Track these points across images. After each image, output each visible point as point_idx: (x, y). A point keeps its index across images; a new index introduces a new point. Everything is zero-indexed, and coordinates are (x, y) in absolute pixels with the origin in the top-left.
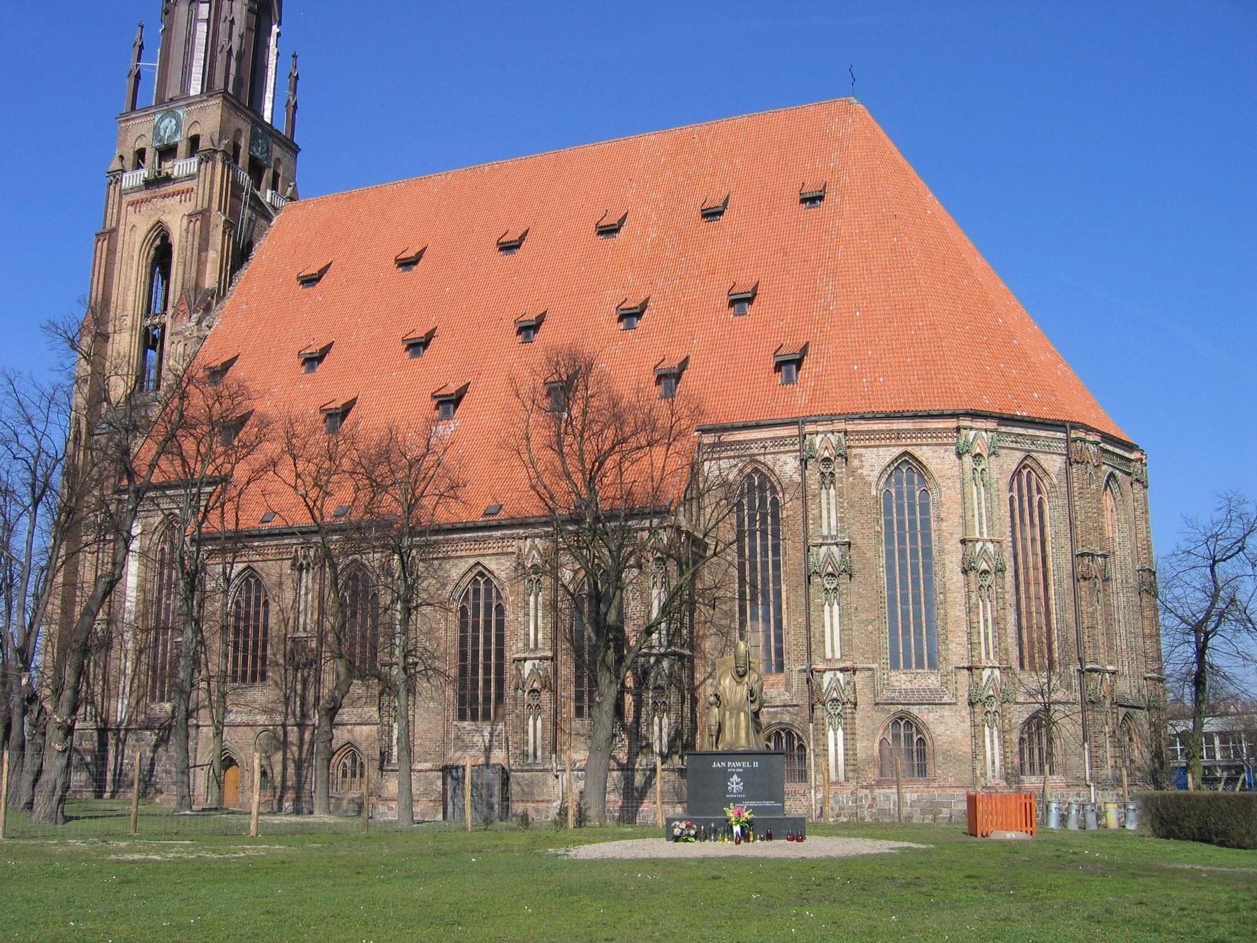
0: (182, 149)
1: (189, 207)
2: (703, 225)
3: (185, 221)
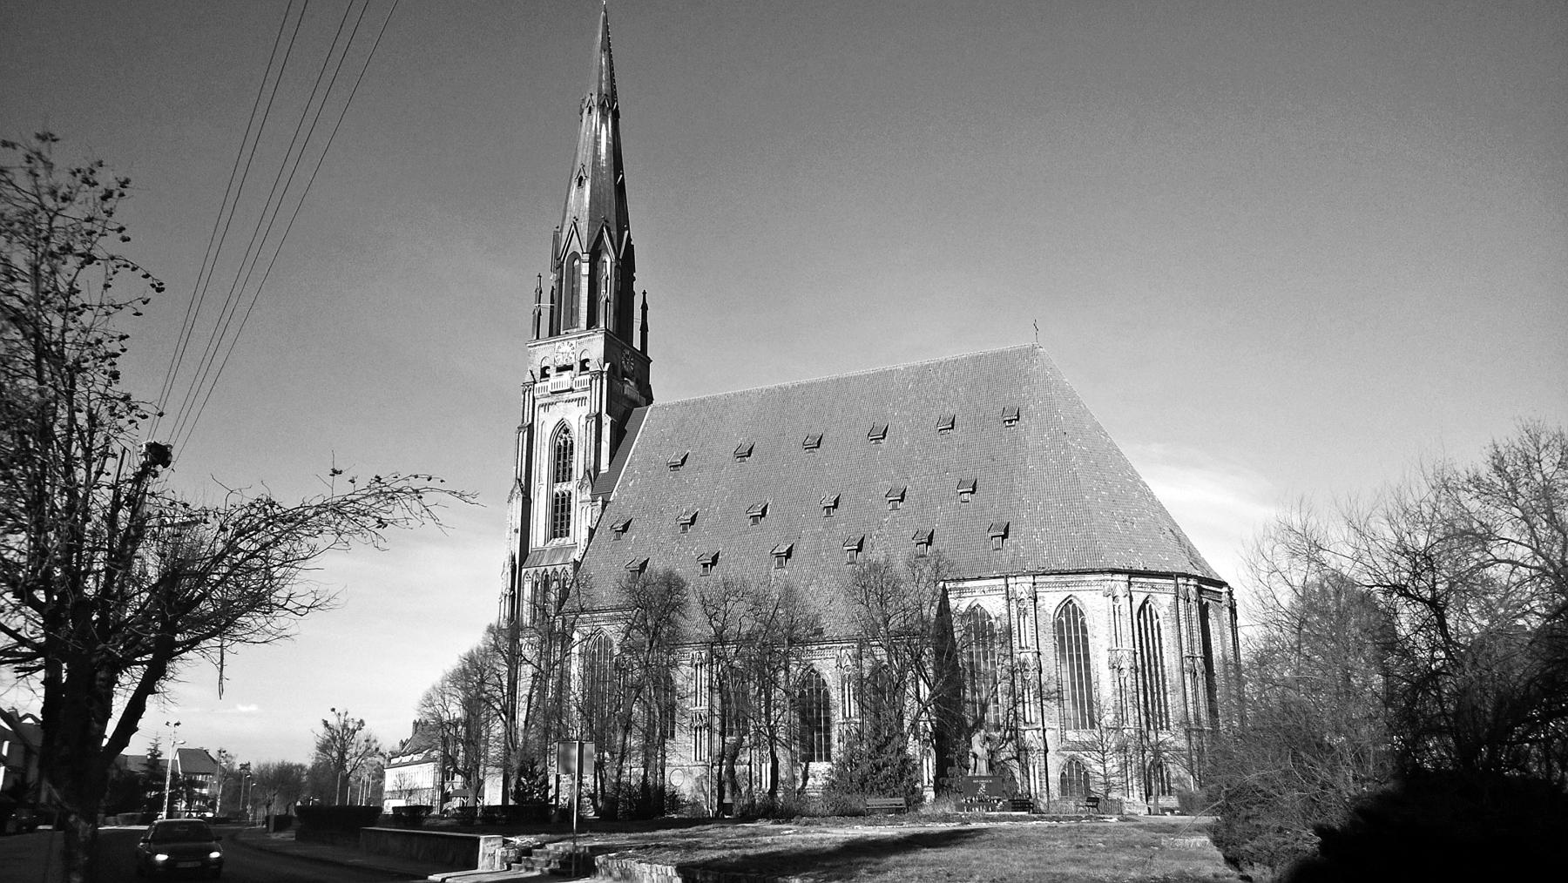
0: (577, 367)
1: (584, 410)
3: (583, 421)
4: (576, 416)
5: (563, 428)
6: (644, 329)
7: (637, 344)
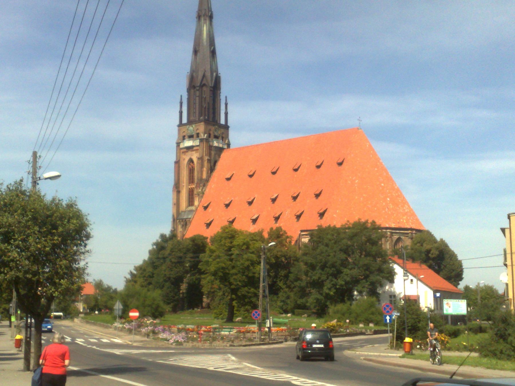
0: (195, 136)
2: (317, 170)
4: (195, 156)
5: (191, 161)
6: (226, 114)
7: (223, 122)
